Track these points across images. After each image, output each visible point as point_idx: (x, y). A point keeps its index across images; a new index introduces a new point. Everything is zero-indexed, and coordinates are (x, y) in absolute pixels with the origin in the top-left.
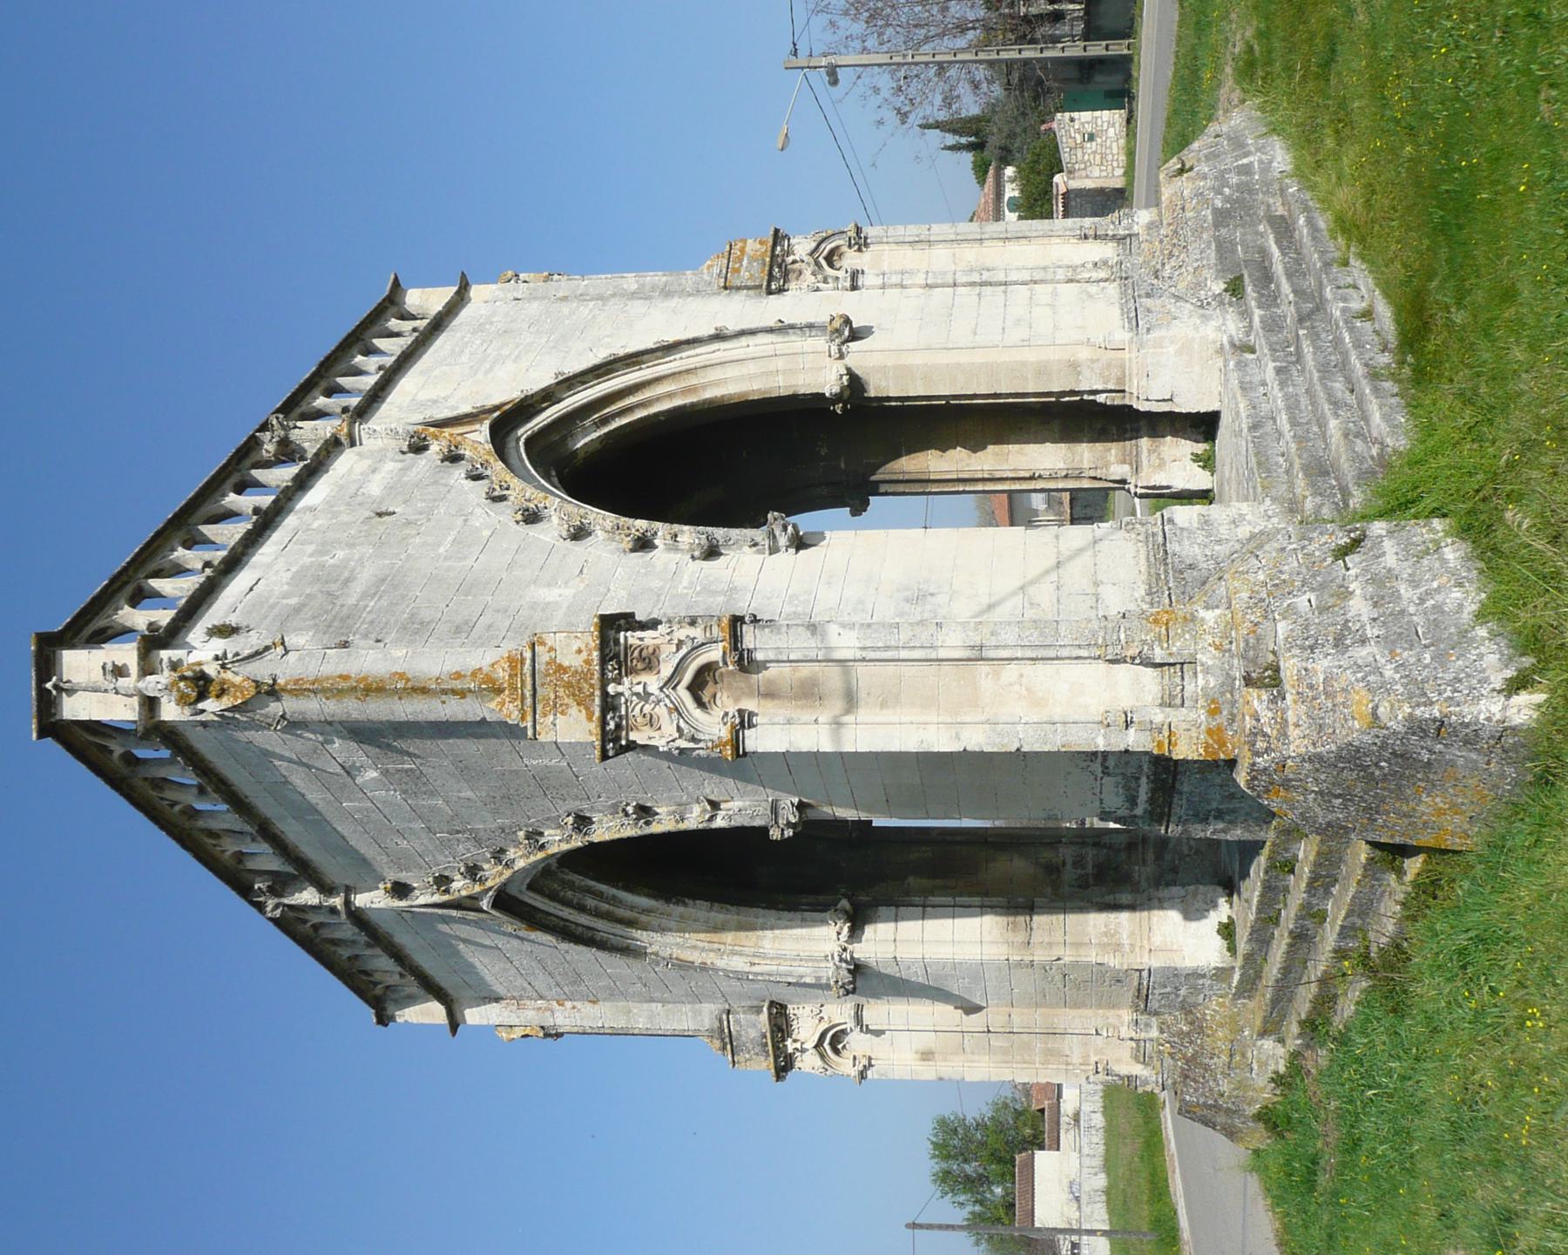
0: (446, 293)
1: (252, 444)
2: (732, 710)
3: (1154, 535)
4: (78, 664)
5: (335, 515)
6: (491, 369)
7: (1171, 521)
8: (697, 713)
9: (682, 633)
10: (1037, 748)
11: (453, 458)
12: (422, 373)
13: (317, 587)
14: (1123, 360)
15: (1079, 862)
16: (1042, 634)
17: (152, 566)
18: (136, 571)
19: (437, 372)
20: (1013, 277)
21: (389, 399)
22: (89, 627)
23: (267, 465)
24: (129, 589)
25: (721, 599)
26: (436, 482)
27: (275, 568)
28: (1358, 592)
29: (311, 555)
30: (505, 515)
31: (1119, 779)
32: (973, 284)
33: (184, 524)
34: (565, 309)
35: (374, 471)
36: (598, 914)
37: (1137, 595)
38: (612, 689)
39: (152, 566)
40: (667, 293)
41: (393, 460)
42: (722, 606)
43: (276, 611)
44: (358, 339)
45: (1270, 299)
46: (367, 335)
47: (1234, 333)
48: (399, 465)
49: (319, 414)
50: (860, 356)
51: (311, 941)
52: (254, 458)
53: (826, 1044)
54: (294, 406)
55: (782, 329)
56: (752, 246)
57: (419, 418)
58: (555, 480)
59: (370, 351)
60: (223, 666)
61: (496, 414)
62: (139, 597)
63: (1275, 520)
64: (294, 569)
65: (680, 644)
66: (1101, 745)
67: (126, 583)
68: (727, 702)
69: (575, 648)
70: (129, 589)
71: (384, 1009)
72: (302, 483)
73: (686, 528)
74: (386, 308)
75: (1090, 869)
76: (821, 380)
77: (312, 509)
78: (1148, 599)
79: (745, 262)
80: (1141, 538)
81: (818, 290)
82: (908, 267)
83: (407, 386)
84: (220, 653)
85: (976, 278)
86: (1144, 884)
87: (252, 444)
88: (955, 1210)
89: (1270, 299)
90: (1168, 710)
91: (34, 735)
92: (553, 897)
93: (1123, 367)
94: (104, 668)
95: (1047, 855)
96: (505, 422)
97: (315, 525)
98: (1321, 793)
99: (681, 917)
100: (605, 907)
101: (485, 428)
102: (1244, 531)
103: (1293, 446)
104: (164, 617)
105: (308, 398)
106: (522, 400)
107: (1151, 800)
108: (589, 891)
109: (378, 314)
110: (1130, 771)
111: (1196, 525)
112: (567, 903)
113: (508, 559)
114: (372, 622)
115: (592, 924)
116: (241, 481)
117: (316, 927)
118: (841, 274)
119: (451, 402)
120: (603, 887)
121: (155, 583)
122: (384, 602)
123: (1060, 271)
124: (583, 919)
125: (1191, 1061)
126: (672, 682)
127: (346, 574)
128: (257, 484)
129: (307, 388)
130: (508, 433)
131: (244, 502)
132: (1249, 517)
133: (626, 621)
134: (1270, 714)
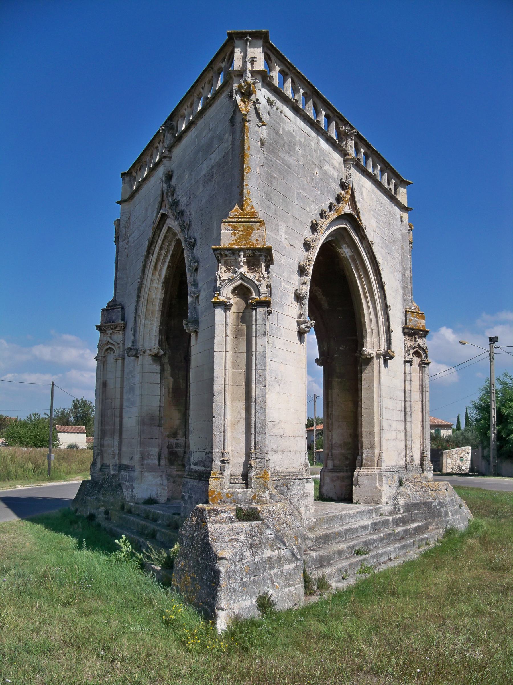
0: (405, 202)
1: (346, 123)
2: (232, 301)
3: (302, 475)
4: (257, 53)
5: (316, 151)
6: (375, 217)
7: (307, 482)
8: (231, 288)
9: (264, 283)
10: (215, 424)
11: (339, 199)
12: (373, 190)
13: (287, 142)
14: (374, 466)
15: (178, 445)
16: (260, 427)
17: (296, 80)
18: (294, 74)
19: (373, 196)
20: (408, 424)
21: (362, 177)
22: (272, 54)
23: (337, 128)
24: (287, 70)
25: (279, 300)
26: (329, 191)
27: (294, 126)
28: (274, 553)
29: (299, 140)
30: (315, 217)
31: (204, 458)
32: (405, 408)
33: (312, 93)
34: (398, 248)
35: (333, 168)
36: (159, 255)
37: (277, 467)
38: (241, 253)
39: (296, 80)
40: (404, 288)
41: (338, 176)
42: (276, 299)
43: (277, 125)
44: (387, 167)
45: (397, 523)
46: (388, 171)
47: (383, 509)
48: (336, 178)
49: (357, 151)
50: (377, 364)
51: (152, 146)
52: (339, 122)
53: (110, 346)
54: (360, 139)
55: (389, 332)
56: (423, 322)
57: (355, 187)
58: (330, 239)
59: (382, 172)
60: (254, 102)
61: (357, 217)
62: (283, 74)
63: (307, 522)
64: (294, 133)
65: (259, 281)
66: (216, 450)
67: (289, 69)
68: (234, 300)
69: (258, 239)
70: (287, 70)
71: (127, 176)
72: (329, 140)
73: (309, 288)
74: (399, 179)
75: (175, 450)
76: (368, 347)
77: (318, 143)
78: (276, 471)
79: (415, 319)
80: (301, 470)
81: (404, 347)
82: (413, 383)
83: (368, 184)
84: (259, 101)
85: (408, 409)
86: (169, 470)
87: (346, 123)
88: (68, 406)
89: (397, 523)
90: (229, 477)
91: (228, 31)
92: (165, 237)
93: (371, 466)
94: (255, 57)
95: (181, 432)
96: (353, 220)
97: (312, 143)
98: (193, 537)
99: (157, 288)
100: (162, 258)
101: (351, 212)
102: (302, 510)
103: (336, 530)
104: (276, 82)
105: (363, 146)
106: (362, 227)
107: (196, 472)
108: (168, 251)
109: (397, 176)
110: (207, 463)
111: (306, 491)
112: (163, 244)
113: (297, 217)
114: (271, 161)
115: (155, 253)
116: (333, 121)
117: (157, 147)
118: (411, 356)
119: (361, 200)
120: (169, 257)
121: (289, 81)
122: (280, 167)
123: (410, 443)
124: (157, 249)
125: (102, 486)
126: (243, 277)
127: (292, 153)
128: (329, 124)
129: (368, 146)
130: (348, 220)
131: (322, 119)
132: (308, 513)
133: (270, 261)
134: (225, 517)
